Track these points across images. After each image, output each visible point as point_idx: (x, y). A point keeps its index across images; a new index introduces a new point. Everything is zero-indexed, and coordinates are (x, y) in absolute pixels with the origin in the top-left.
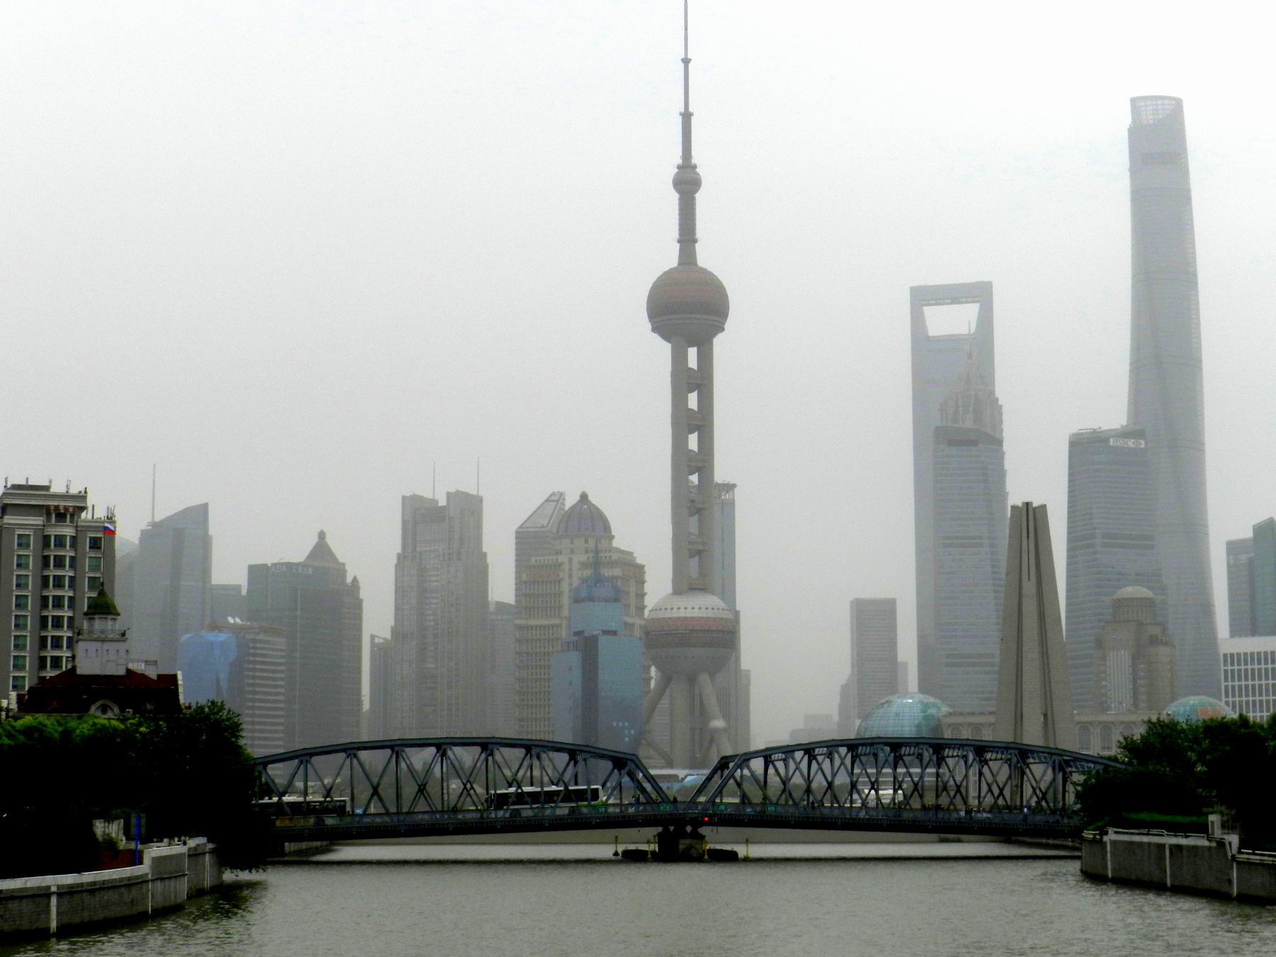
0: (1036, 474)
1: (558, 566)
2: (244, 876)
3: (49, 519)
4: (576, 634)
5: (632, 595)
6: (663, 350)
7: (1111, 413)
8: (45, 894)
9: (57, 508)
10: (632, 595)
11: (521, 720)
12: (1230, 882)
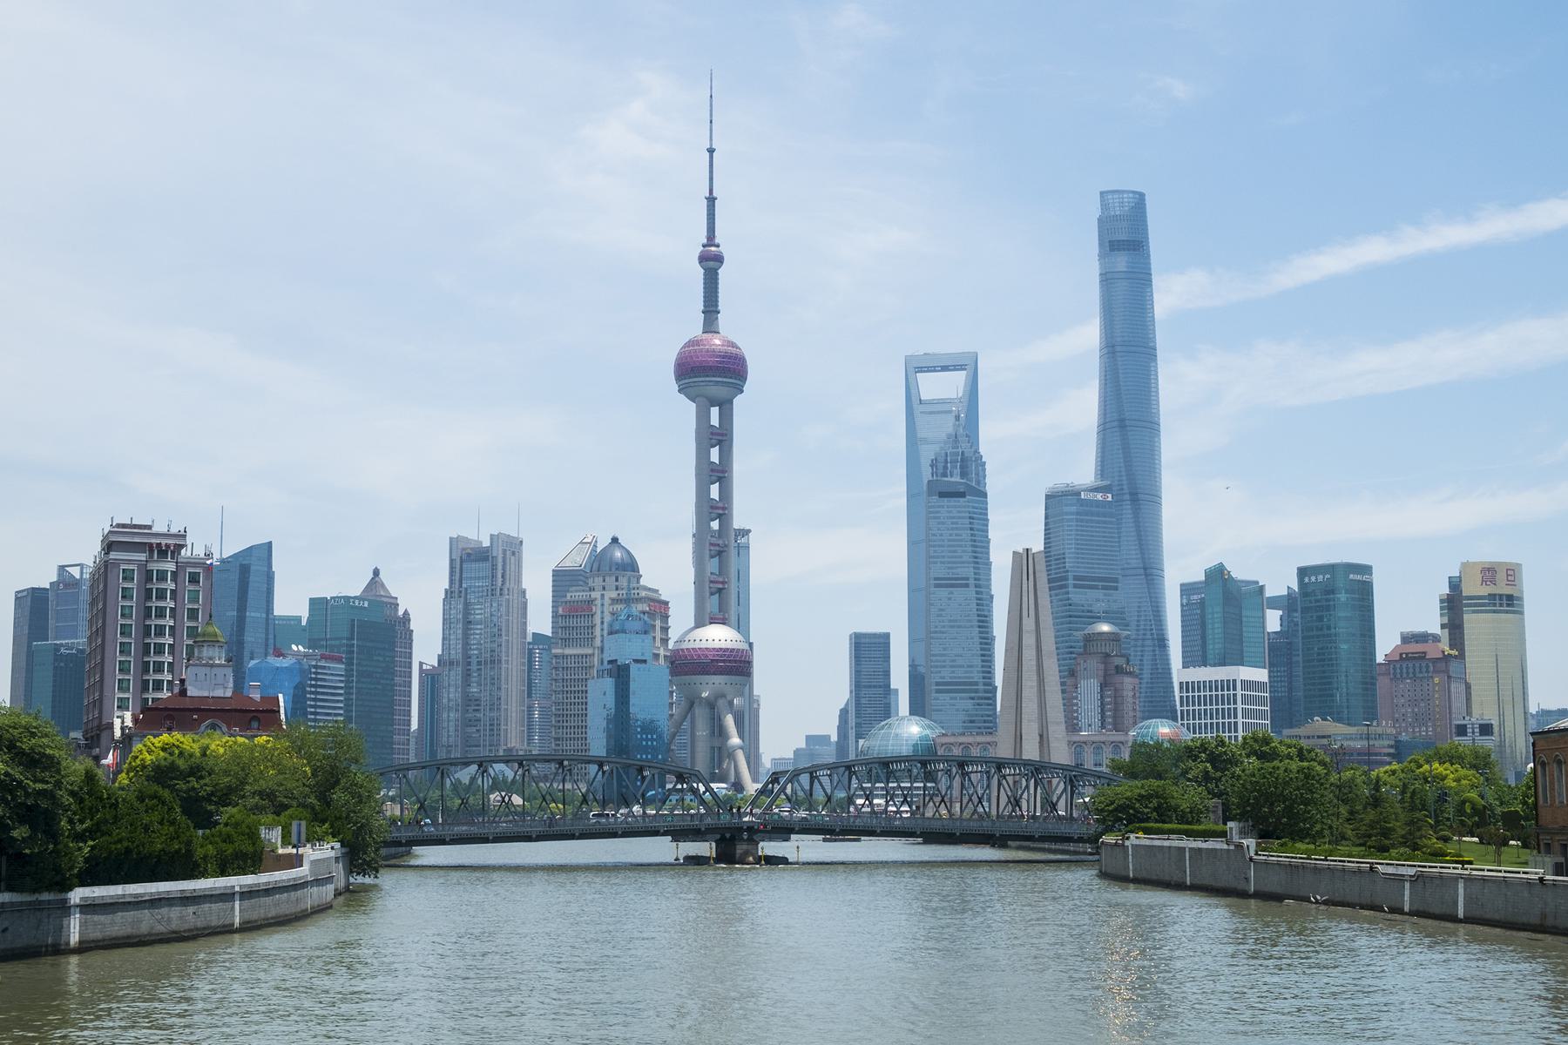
0: (1015, 528)
1: (591, 602)
2: (368, 880)
3: (151, 556)
4: (610, 662)
5: (658, 628)
6: (687, 409)
7: (1082, 471)
8: (1400, 879)
9: (159, 545)
10: (658, 628)
11: (557, 739)
12: (1247, 879)
